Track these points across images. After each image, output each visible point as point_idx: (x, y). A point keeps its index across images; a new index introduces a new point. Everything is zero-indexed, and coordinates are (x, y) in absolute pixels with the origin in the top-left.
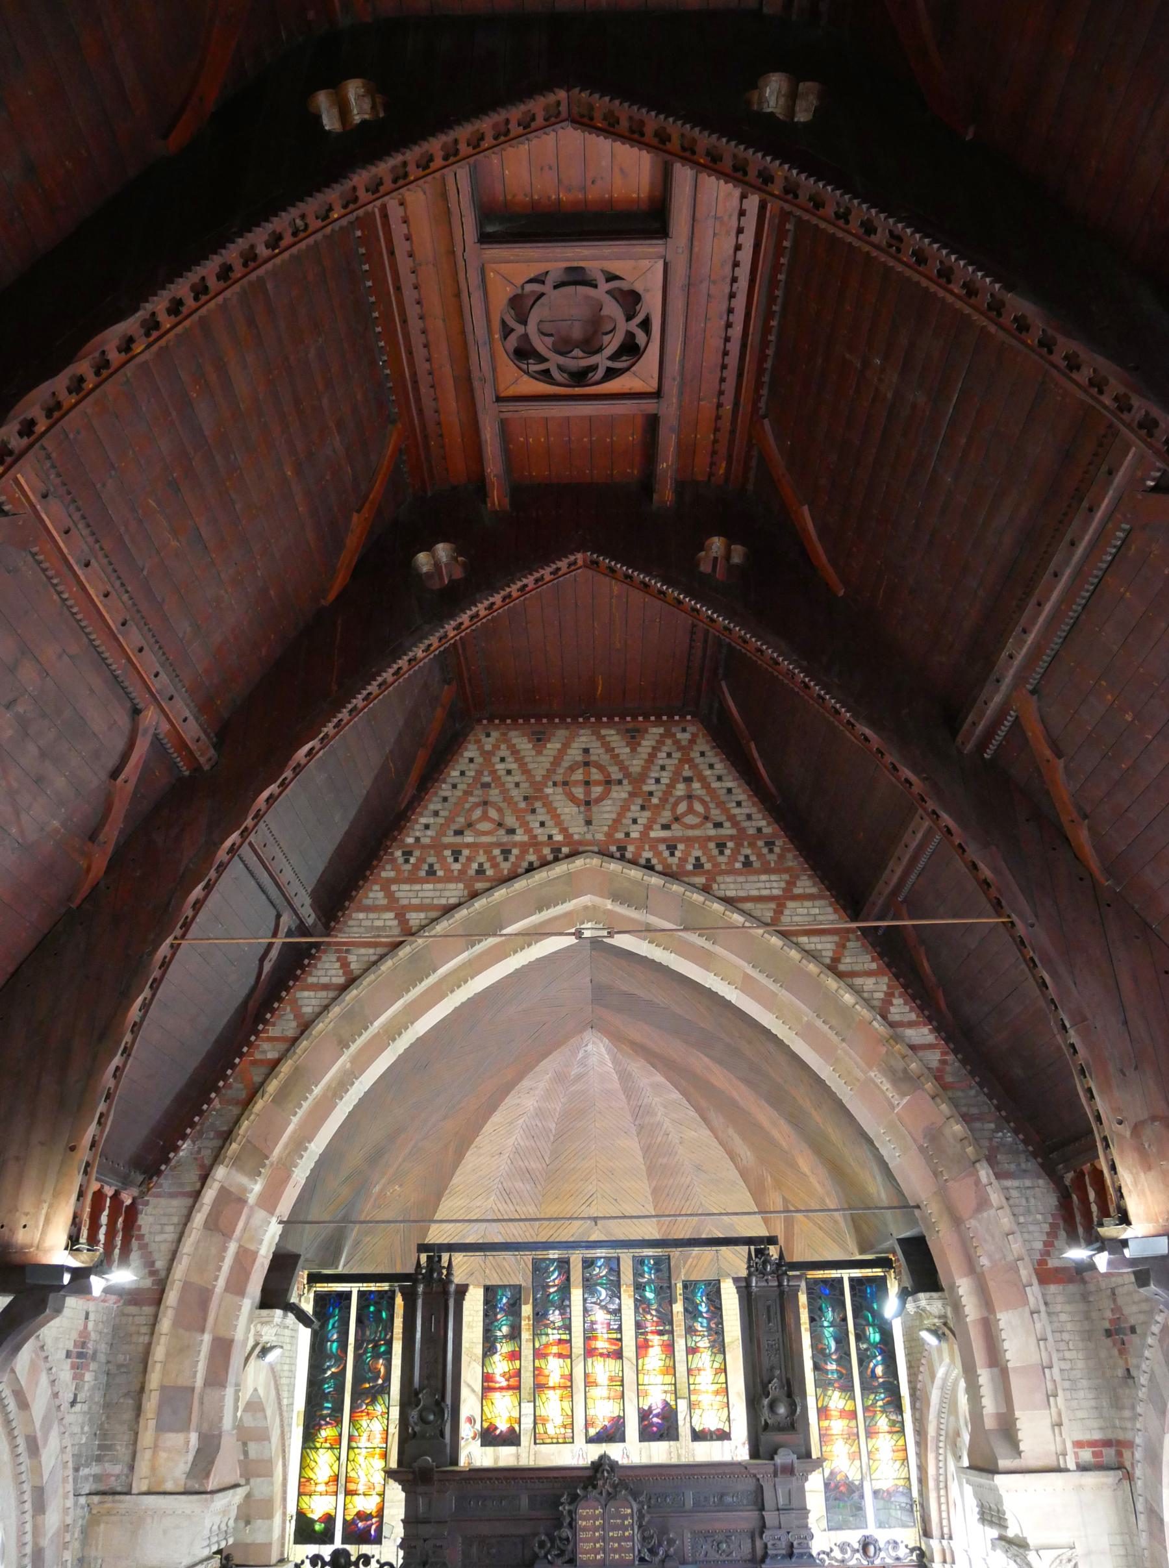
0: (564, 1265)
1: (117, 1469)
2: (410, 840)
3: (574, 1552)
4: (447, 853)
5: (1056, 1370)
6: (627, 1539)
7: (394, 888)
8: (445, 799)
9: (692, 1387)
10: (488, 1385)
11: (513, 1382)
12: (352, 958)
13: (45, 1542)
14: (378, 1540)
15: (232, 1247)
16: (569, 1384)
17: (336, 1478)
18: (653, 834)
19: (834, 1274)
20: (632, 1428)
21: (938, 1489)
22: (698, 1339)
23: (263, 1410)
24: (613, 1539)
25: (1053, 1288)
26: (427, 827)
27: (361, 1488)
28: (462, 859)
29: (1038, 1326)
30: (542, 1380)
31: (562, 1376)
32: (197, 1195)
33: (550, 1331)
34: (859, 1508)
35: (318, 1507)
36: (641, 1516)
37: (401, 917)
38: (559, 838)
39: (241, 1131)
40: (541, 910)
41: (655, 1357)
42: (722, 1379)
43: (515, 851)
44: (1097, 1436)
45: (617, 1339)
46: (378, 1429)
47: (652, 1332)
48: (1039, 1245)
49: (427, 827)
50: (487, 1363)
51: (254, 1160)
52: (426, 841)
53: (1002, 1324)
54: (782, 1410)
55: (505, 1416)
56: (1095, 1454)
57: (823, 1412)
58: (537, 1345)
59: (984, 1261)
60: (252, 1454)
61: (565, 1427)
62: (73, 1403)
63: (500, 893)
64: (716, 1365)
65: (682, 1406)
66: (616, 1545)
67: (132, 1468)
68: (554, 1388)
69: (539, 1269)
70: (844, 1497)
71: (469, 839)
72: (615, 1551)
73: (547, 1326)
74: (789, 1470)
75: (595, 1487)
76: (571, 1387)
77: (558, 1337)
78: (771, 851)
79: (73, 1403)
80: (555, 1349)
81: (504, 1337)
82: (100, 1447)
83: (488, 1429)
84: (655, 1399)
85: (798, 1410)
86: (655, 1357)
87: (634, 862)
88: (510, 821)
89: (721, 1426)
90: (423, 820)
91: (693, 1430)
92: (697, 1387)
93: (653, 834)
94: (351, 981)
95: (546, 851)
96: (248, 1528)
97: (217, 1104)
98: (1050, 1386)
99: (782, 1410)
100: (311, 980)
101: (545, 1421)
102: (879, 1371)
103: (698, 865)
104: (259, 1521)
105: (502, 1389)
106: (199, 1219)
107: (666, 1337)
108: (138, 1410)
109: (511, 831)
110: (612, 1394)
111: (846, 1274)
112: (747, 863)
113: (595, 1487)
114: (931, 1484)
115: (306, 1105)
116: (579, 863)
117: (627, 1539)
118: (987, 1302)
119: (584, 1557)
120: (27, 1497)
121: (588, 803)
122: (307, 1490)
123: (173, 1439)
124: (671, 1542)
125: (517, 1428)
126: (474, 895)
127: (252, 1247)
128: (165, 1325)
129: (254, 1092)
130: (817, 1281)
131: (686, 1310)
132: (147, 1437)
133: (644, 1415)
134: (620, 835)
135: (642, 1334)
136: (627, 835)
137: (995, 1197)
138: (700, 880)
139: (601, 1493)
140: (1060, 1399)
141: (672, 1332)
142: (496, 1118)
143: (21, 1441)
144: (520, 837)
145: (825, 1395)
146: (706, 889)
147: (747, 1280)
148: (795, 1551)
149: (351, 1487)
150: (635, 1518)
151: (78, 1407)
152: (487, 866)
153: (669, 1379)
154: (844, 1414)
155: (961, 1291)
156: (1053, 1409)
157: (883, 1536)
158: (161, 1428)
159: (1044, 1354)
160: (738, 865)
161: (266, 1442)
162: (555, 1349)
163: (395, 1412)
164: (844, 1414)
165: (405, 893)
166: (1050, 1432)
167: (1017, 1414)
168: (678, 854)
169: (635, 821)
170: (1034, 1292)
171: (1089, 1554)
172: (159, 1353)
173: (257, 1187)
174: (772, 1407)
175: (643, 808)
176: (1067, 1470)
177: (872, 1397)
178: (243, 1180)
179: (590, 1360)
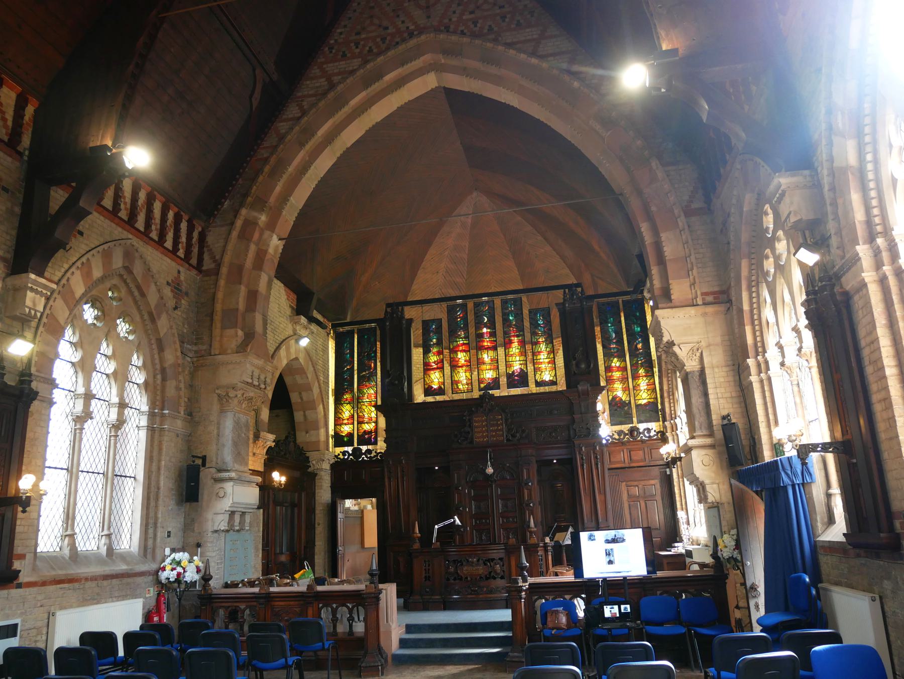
0: (464, 307)
1: (204, 347)
2: (332, 42)
3: (472, 439)
4: (352, 45)
5: (693, 257)
6: (500, 430)
7: (325, 66)
8: (350, 18)
10: (427, 368)
12: (305, 103)
13: (166, 365)
15: (253, 248)
17: (352, 417)
18: (464, 17)
19: (613, 299)
20: (503, 381)
21: (669, 396)
23: (305, 373)
24: (493, 431)
25: (693, 219)
26: (341, 33)
27: (366, 420)
28: (360, 47)
29: (684, 237)
30: (455, 363)
32: (232, 224)
35: (346, 429)
36: (506, 420)
37: (329, 80)
38: (412, 27)
39: (253, 191)
40: (403, 65)
41: (515, 349)
42: (552, 356)
43: (388, 38)
44: (716, 289)
46: (372, 393)
47: (514, 336)
48: (686, 198)
49: (341, 33)
51: (260, 204)
52: (341, 40)
53: (663, 239)
54: (583, 366)
55: (436, 381)
56: (715, 298)
57: (609, 369)
59: (654, 209)
60: (305, 398)
61: (467, 384)
62: (176, 308)
63: (381, 59)
65: (530, 368)
67: (211, 346)
68: (462, 367)
69: (451, 311)
71: (363, 36)
72: (493, 436)
74: (586, 393)
75: (482, 407)
78: (532, 16)
79: (176, 308)
82: (197, 339)
84: (516, 367)
86: (515, 349)
87: (455, 32)
88: (385, 23)
90: (339, 31)
91: (536, 381)
93: (464, 17)
94: (304, 113)
95: (406, 35)
97: (240, 181)
98: (689, 266)
99: (583, 366)
100: (284, 117)
101: (457, 382)
102: (640, 346)
103: (490, 29)
105: (435, 369)
106: (235, 234)
108: (212, 320)
109: (387, 28)
111: (620, 299)
112: (519, 24)
113: (482, 407)
114: (666, 395)
115: (285, 177)
116: (423, 37)
117: (500, 430)
118: (656, 232)
119: (478, 440)
120: (153, 341)
121: (428, 7)
123: (230, 332)
124: (523, 431)
126: (366, 62)
127: (264, 248)
128: (222, 282)
129: (258, 172)
130: (603, 304)
131: (531, 324)
132: (217, 331)
133: (510, 376)
134: (446, 21)
136: (450, 20)
137: (660, 174)
138: (493, 36)
140: (695, 271)
141: (524, 335)
142: (432, 251)
143: (146, 317)
144: (391, 30)
146: (495, 40)
147: (563, 304)
149: (361, 420)
151: (178, 312)
152: (373, 47)
153: (522, 358)
154: (619, 369)
155: (643, 230)
156: (691, 277)
157: (642, 427)
158: (223, 328)
159: (687, 250)
160: (513, 26)
162: (461, 348)
163: (379, 383)
164: (619, 369)
165: (330, 68)
166: (689, 289)
167: (670, 282)
168: (479, 25)
169: (454, 12)
170: (682, 221)
171: (709, 346)
172: (220, 295)
173: (263, 218)
174: (577, 365)
175: (459, 5)
176: (698, 305)
178: (255, 214)
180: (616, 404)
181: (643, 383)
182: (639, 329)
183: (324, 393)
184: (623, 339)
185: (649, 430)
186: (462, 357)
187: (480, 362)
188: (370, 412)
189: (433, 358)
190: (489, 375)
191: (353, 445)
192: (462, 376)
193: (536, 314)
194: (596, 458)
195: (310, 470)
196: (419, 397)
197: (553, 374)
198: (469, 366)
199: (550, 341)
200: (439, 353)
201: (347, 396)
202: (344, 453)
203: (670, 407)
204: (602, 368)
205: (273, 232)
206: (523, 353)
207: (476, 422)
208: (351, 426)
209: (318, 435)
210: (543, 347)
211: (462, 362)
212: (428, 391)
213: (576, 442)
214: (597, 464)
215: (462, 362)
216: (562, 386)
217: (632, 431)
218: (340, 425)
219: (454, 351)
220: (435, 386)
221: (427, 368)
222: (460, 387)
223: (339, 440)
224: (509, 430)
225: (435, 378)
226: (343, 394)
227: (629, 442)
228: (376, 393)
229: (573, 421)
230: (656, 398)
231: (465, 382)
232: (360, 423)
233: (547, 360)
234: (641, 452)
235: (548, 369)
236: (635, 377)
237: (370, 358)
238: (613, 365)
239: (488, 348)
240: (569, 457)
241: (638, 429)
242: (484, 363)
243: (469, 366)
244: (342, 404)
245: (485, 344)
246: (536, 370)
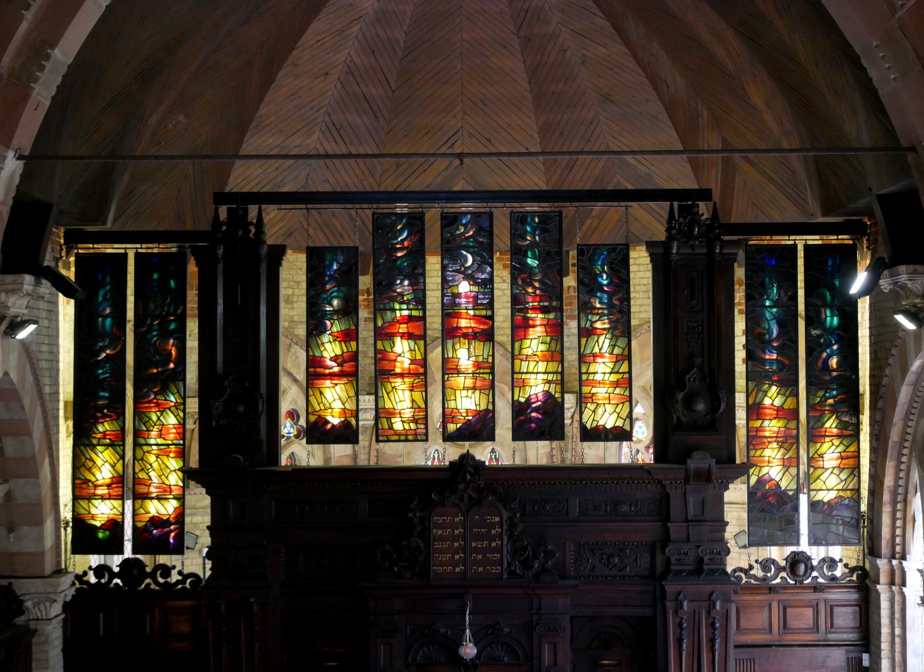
0: (416, 223)
9: (584, 377)
10: (315, 371)
11: (347, 367)
14: (179, 548)
16: (421, 370)
21: (894, 503)
22: (596, 318)
23: (19, 400)
24: (477, 550)
30: (386, 365)
31: (413, 361)
33: (397, 306)
34: (791, 523)
35: (102, 511)
36: (512, 526)
41: (535, 342)
45: (486, 317)
46: (171, 421)
47: (534, 309)
50: (313, 344)
54: (701, 406)
55: (337, 406)
57: (755, 410)
58: (380, 323)
61: (415, 421)
64: (617, 351)
66: (480, 557)
68: (401, 375)
69: (383, 228)
70: (772, 512)
72: (478, 563)
73: (393, 299)
74: (705, 477)
76: (425, 374)
77: (406, 313)
80: (403, 328)
81: (335, 312)
83: (316, 422)
84: (536, 387)
85: (723, 406)
86: (535, 342)
89: (620, 423)
91: (583, 427)
92: (591, 377)
96: (12, 535)
99: (701, 406)
102: (834, 362)
104: (26, 528)
105: (332, 376)
107: (552, 316)
110: (479, 384)
111: (800, 241)
114: (886, 497)
119: (440, 569)
122: (84, 493)
124: (549, 555)
125: (353, 422)
131: (580, 282)
133: (520, 410)
135: (520, 311)
139: (462, 499)
145: (759, 390)
147: (666, 245)
148: (705, 567)
150: (505, 527)
153: (553, 366)
154: (780, 413)
161: (26, 438)
162: (403, 328)
164: (780, 413)
174: (688, 402)
177: (821, 393)
179: (450, 343)
180: (765, 496)
181: (830, 452)
182: (836, 321)
183: (52, 422)
184: (796, 342)
185: (832, 563)
186: (403, 351)
187: (449, 368)
188: (165, 471)
189: (330, 349)
190: (467, 402)
191: (121, 551)
192: (401, 398)
193: (592, 262)
194: (713, 625)
195: (20, 620)
196: (298, 453)
197: (624, 414)
198: (420, 374)
199: (622, 328)
200: (349, 336)
201: (104, 427)
202: (101, 570)
203: (893, 527)
204: (741, 416)
205: (8, 147)
206: (556, 354)
207: (439, 527)
208: (117, 503)
209: (41, 537)
210: (604, 343)
211: (404, 363)
212: (317, 432)
213: (671, 588)
214: (712, 641)
215: (404, 363)
216: (639, 448)
217: (796, 562)
218: (90, 498)
219: (384, 334)
220: (335, 421)
221: (315, 371)
222: (398, 425)
223: (86, 537)
224: (515, 551)
225: (334, 399)
226: (96, 421)
227: (784, 587)
228: (182, 425)
229: (666, 539)
230: (858, 490)
231: (408, 414)
232: (140, 497)
233: (614, 378)
234: (809, 612)
235: (618, 412)
236: (815, 436)
237: (165, 335)
238: (767, 401)
239: (473, 336)
240: (648, 612)
241: (809, 559)
242: (458, 372)
243: (420, 374)
244: (93, 447)
245: (463, 323)
246: (582, 400)
